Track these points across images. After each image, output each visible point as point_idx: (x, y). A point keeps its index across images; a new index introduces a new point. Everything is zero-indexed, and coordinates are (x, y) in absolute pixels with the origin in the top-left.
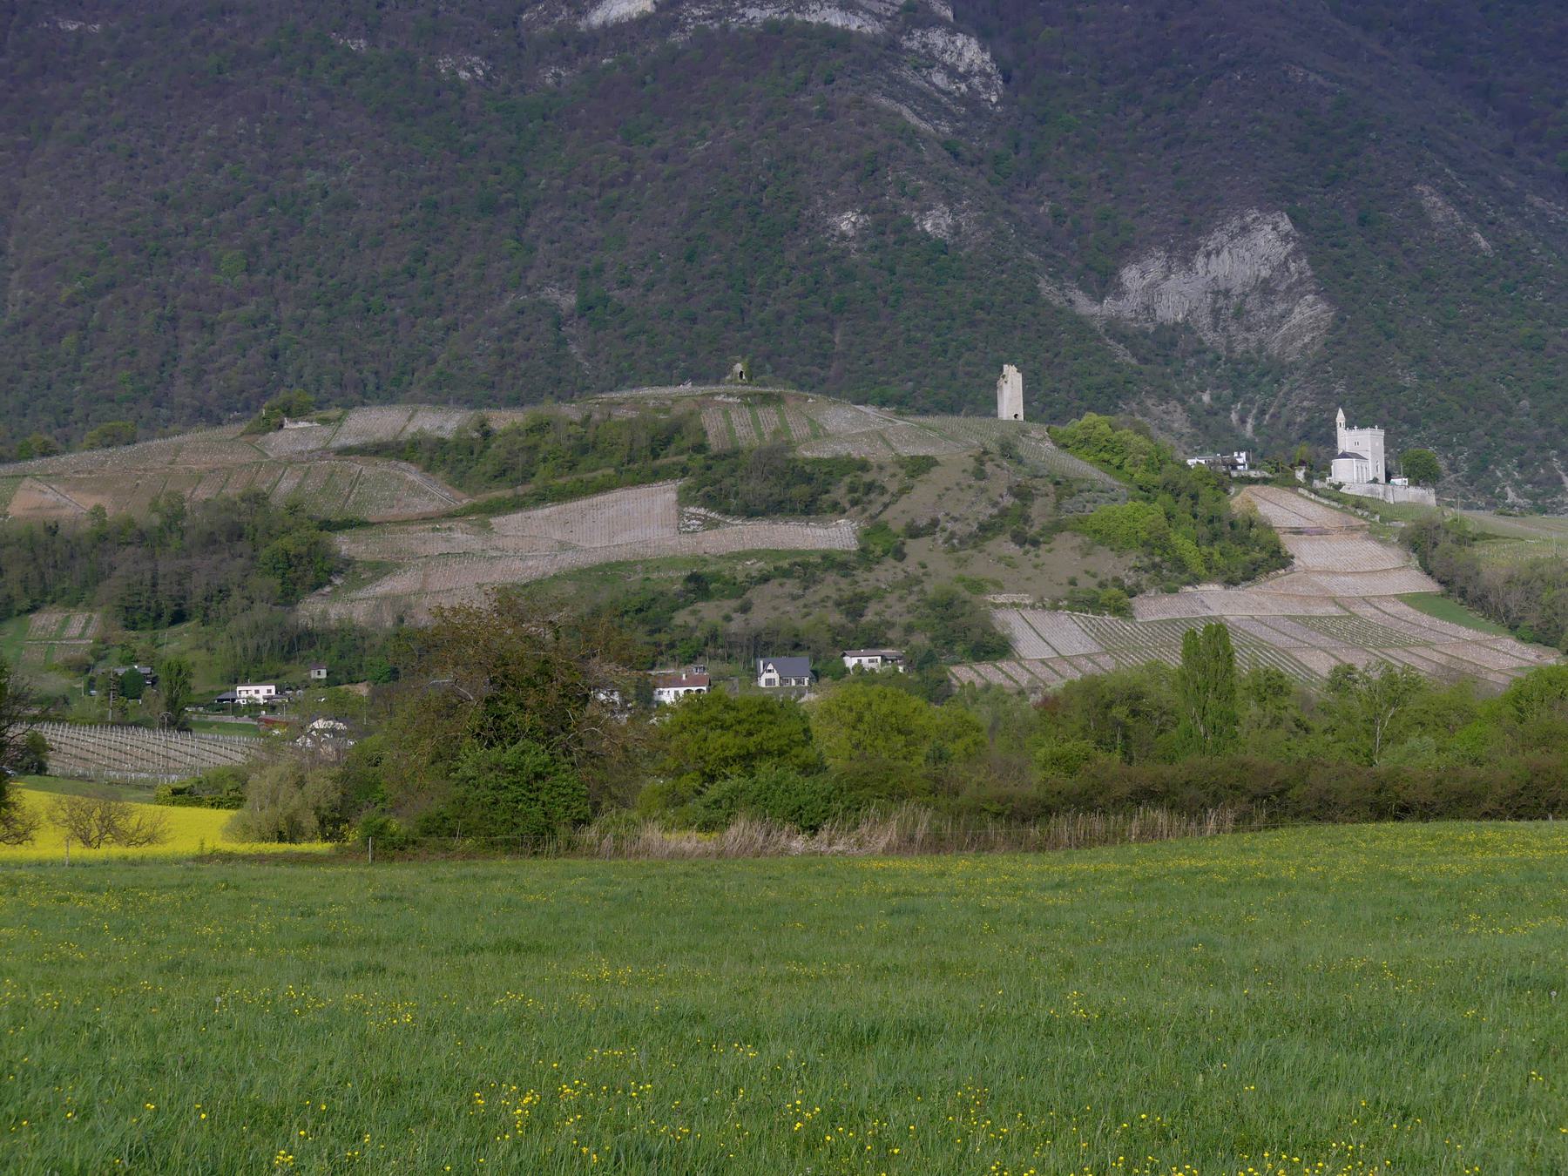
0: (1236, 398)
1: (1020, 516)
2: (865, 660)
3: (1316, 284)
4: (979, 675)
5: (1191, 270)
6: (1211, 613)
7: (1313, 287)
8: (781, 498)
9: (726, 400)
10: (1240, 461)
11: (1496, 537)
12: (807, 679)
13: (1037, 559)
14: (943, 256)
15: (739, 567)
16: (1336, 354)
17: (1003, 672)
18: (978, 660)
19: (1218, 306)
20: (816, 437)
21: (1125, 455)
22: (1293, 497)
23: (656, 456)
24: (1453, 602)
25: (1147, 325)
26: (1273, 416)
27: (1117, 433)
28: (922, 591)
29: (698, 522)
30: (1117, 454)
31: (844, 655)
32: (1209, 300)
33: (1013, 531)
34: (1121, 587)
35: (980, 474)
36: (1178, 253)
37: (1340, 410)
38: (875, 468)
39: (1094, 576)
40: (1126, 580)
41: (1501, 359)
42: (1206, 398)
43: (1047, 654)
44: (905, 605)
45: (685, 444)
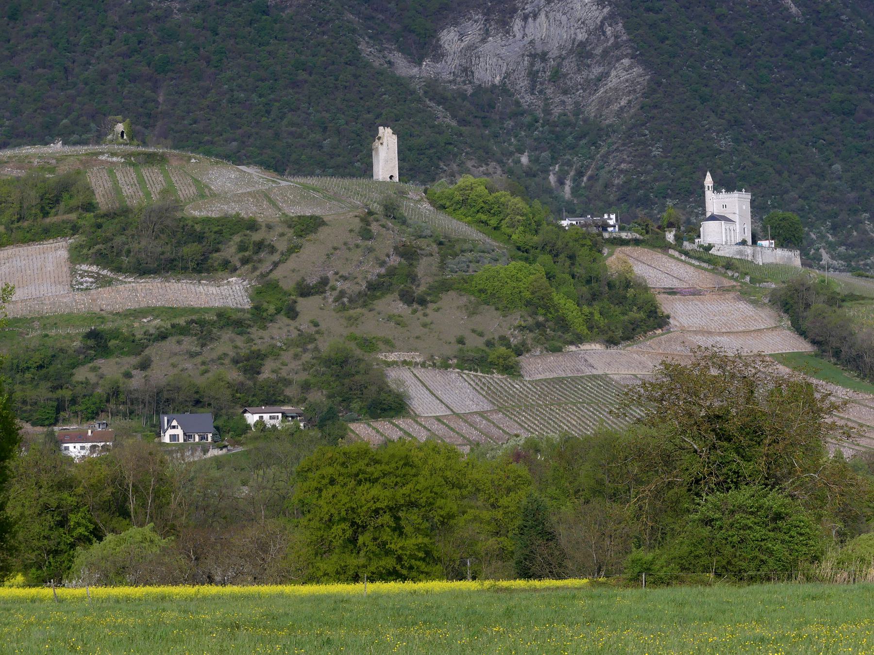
0: (554, 160)
1: (408, 276)
2: (266, 417)
3: (632, 47)
4: (378, 432)
5: (508, 33)
6: (595, 372)
7: (629, 51)
8: (172, 257)
9: (110, 159)
10: (612, 222)
11: (863, 298)
12: (210, 436)
13: (425, 318)
14: (265, 17)
15: (136, 325)
16: (653, 118)
17: (401, 429)
18: (375, 416)
19: (535, 68)
20: (202, 196)
21: (502, 216)
22: (665, 258)
23: (46, 214)
24: (827, 363)
25: (465, 87)
26: (591, 178)
27: (494, 195)
28: (316, 349)
29: (91, 280)
30: (494, 214)
31: (245, 412)
32: (526, 62)
33: (402, 290)
34: (508, 346)
35: (366, 234)
36: (496, 16)
37: (708, 174)
38: (264, 228)
39: (481, 335)
40: (512, 339)
41: (813, 124)
42: (524, 160)
43: (442, 411)
44: (300, 362)
45: (74, 202)
